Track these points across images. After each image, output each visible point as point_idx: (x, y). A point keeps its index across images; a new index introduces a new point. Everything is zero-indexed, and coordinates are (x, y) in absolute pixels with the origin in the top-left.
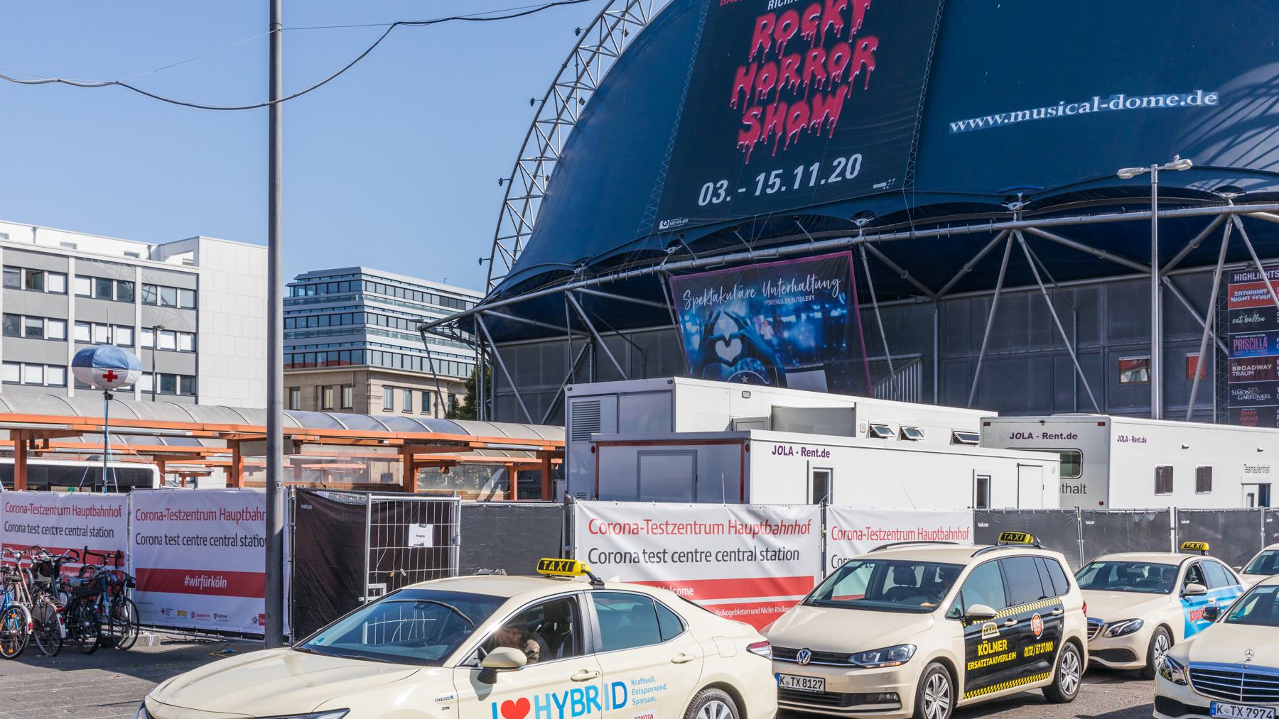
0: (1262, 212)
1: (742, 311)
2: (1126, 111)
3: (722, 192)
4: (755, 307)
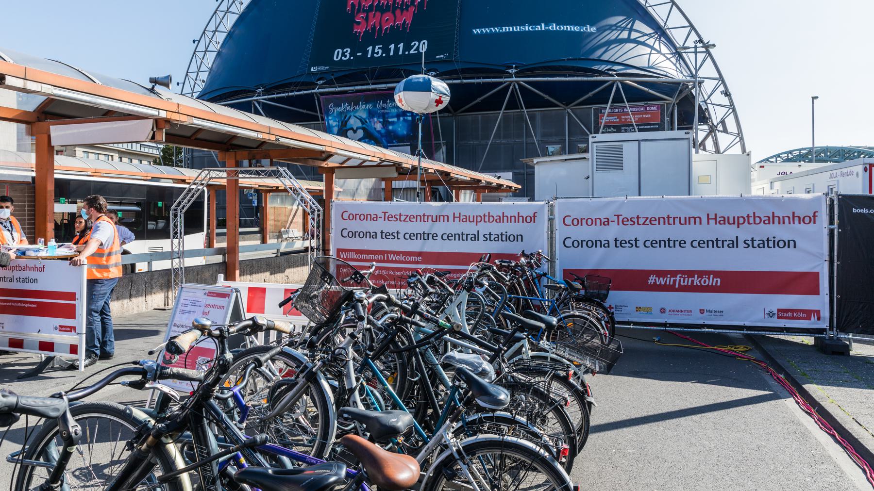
0: (628, 81)
1: (364, 115)
2: (557, 31)
3: (348, 54)
4: (371, 114)
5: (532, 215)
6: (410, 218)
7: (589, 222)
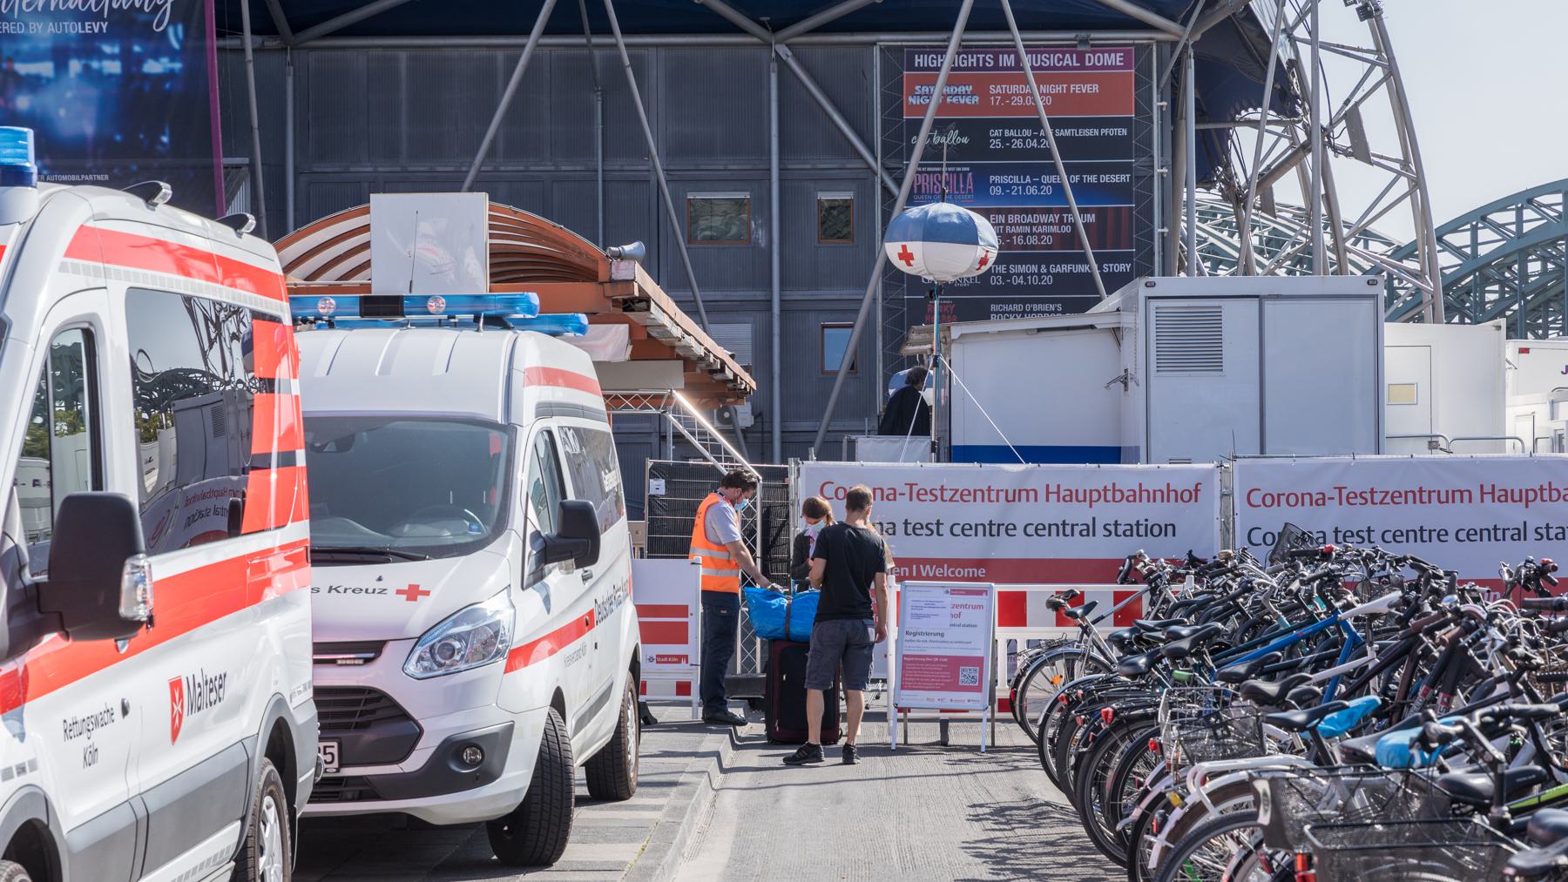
5: (1192, 488)
6: (963, 495)
7: (1292, 500)
